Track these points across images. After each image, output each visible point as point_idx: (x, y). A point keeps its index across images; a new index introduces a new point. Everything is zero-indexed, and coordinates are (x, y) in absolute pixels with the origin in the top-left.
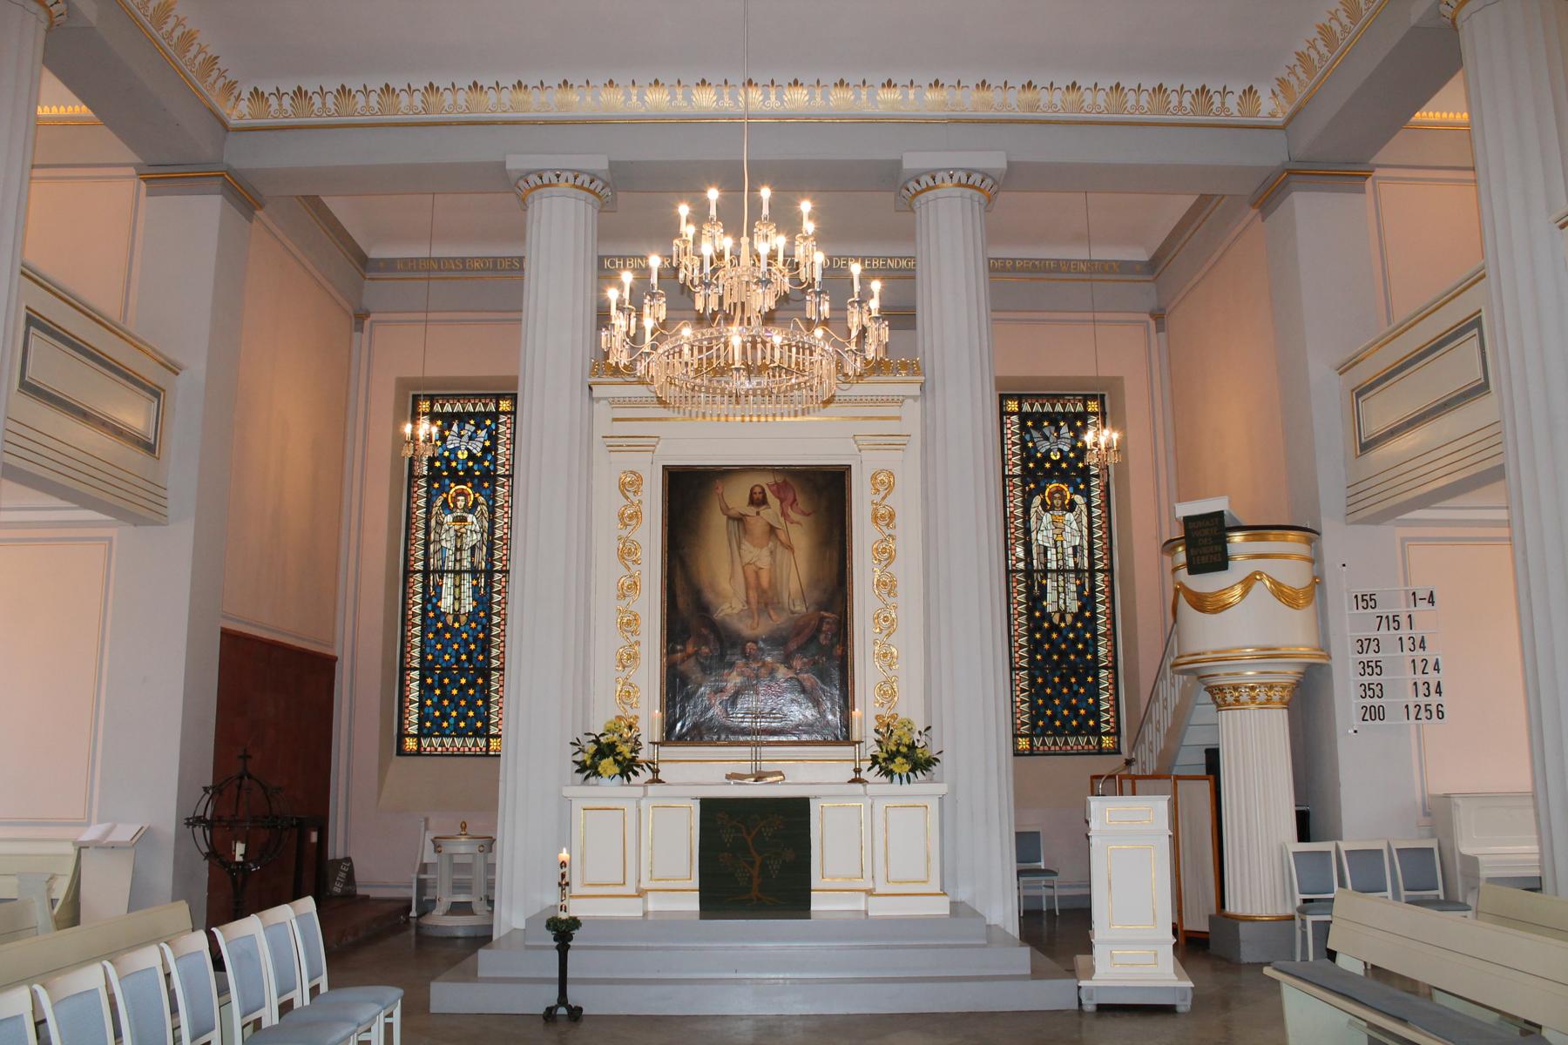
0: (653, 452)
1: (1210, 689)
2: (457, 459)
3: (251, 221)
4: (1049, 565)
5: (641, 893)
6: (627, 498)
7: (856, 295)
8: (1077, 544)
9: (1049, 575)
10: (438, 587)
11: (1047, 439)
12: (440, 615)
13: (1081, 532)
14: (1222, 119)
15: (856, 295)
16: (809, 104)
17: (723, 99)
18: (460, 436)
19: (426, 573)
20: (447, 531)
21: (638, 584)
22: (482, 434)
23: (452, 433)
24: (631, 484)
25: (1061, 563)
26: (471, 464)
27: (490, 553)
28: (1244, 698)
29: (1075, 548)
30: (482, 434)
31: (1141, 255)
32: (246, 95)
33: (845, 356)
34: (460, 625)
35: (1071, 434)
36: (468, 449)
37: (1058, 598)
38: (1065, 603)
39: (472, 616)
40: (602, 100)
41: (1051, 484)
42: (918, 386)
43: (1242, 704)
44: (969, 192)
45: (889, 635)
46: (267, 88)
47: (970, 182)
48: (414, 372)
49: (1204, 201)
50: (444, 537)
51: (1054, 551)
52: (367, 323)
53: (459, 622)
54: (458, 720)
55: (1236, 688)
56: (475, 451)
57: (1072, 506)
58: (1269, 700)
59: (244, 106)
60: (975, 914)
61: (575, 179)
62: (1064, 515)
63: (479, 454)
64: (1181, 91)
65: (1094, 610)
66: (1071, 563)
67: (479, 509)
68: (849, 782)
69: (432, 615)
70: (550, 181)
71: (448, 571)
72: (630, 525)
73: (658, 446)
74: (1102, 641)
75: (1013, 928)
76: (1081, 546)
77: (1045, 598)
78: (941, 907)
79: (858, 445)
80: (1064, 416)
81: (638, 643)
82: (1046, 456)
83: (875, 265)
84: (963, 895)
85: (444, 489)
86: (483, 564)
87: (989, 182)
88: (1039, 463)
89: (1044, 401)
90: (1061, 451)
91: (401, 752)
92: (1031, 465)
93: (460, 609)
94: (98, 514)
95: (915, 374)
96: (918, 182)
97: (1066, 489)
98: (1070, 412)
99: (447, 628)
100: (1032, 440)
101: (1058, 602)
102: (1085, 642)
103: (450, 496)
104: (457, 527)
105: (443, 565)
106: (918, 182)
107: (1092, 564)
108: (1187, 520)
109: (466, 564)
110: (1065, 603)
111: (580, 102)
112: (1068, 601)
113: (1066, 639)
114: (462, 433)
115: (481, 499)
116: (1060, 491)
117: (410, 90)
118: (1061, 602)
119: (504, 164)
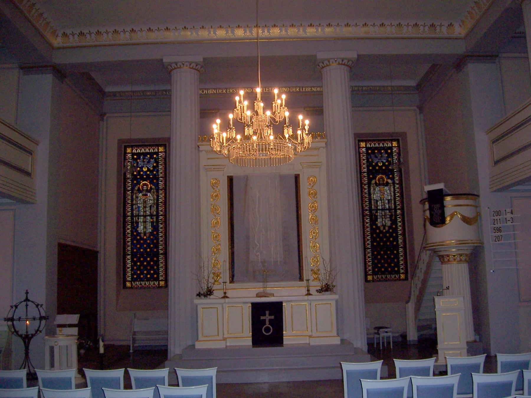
0: (223, 171)
1: (439, 256)
2: (143, 171)
3: (62, 82)
4: (378, 207)
5: (225, 339)
6: (214, 189)
7: (301, 127)
8: (390, 198)
9: (378, 211)
10: (137, 223)
11: (376, 157)
12: (139, 234)
13: (391, 194)
14: (440, 35)
15: (301, 127)
16: (280, 34)
17: (247, 32)
18: (144, 162)
19: (132, 216)
20: (140, 200)
21: (219, 222)
22: (152, 161)
23: (141, 161)
24: (216, 183)
25: (383, 206)
26: (148, 173)
27: (157, 208)
28: (451, 259)
29: (389, 200)
30: (152, 161)
31: (412, 83)
32: (60, 35)
33: (297, 146)
34: (146, 237)
35: (386, 155)
36: (147, 167)
37: (382, 220)
38: (385, 222)
39: (151, 234)
40: (199, 34)
41: (379, 175)
42: (325, 143)
43: (450, 262)
44: (343, 66)
45: (316, 239)
46: (68, 32)
47: (343, 63)
48: (125, 136)
49: (434, 66)
50: (139, 202)
51: (380, 202)
52: (105, 118)
53: (146, 236)
54: (147, 274)
55: (448, 256)
56: (150, 168)
57: (387, 184)
58: (461, 260)
59: (59, 39)
60: (350, 343)
61: (190, 65)
62: (384, 188)
63: (152, 169)
64: (424, 26)
65: (396, 224)
66: (387, 206)
67: (152, 191)
68: (222, 298)
69: (135, 233)
70: (180, 66)
71: (141, 216)
72: (215, 199)
73: (225, 169)
74: (400, 237)
75: (365, 348)
76: (391, 199)
77: (377, 221)
78: (337, 341)
79: (302, 167)
80: (383, 148)
81: (220, 244)
82: (377, 164)
83: (307, 90)
84: (346, 336)
85: (138, 183)
86: (155, 213)
87: (350, 62)
88: (374, 167)
89: (375, 143)
90: (382, 162)
91: (125, 287)
92: (371, 168)
93: (146, 231)
94: (9, 200)
95: (323, 138)
96: (323, 63)
97: (384, 177)
98: (386, 147)
99: (141, 239)
100: (371, 157)
101: (382, 222)
102: (393, 237)
103: (140, 186)
104: (144, 198)
105: (139, 214)
106: (323, 63)
107: (395, 207)
108: (429, 192)
109: (148, 213)
110: (385, 222)
111: (190, 35)
112: (386, 221)
113: (386, 237)
114: (145, 160)
115: (153, 187)
116: (382, 178)
117: (124, 31)
118: (384, 222)
119: (162, 60)
